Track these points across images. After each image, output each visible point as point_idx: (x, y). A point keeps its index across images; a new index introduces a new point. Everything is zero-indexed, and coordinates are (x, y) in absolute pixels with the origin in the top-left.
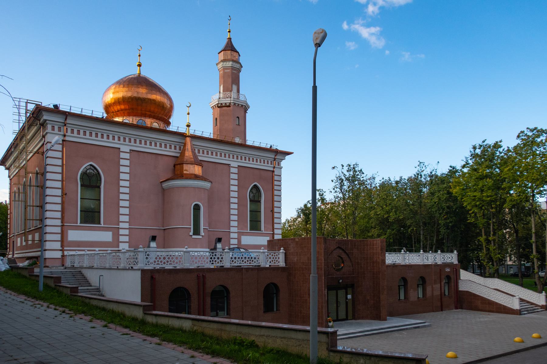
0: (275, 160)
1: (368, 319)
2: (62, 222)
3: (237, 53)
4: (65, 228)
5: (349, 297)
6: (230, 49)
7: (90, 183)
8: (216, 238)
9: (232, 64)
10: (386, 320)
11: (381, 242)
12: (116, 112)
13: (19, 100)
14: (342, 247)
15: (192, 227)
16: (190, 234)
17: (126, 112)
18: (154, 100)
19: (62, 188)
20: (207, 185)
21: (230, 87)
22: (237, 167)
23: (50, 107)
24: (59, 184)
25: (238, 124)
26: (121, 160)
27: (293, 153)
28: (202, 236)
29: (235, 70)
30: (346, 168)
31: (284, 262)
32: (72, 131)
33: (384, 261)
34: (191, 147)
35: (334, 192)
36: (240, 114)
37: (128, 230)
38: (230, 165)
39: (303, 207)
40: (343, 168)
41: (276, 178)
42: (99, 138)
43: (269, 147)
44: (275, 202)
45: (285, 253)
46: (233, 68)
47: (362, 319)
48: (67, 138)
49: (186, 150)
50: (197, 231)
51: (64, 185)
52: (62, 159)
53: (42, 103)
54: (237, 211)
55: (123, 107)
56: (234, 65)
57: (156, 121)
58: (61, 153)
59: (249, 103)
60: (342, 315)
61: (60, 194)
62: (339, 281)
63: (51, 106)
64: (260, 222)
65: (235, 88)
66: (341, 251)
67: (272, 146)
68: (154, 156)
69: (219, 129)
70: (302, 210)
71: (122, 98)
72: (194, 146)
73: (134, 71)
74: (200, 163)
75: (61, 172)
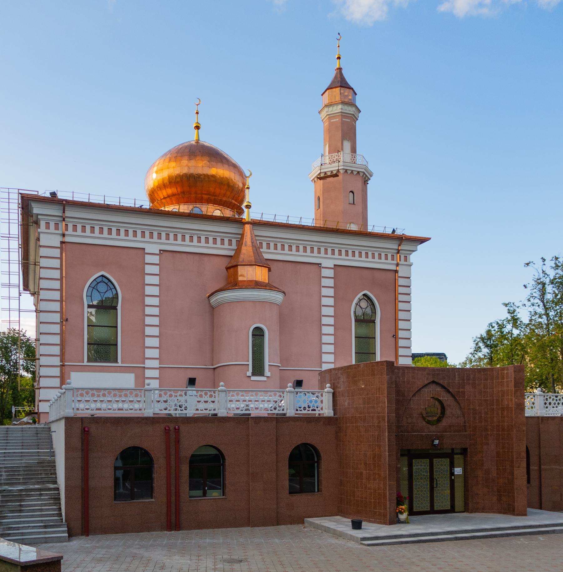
0: (398, 253)
1: (494, 512)
2: (61, 361)
3: (351, 90)
4: (67, 368)
5: (458, 471)
6: (339, 85)
7: (102, 304)
8: (295, 381)
9: (342, 109)
10: (525, 515)
11: (514, 371)
12: (161, 199)
13: (7, 190)
14: (441, 382)
15: (250, 363)
16: (248, 375)
17: (173, 198)
18: (213, 176)
19: (61, 312)
20: (277, 297)
21: (340, 144)
22: (333, 266)
23: (46, 196)
24: (56, 306)
25: (353, 203)
26: (146, 266)
27: (430, 239)
28: (267, 377)
29: (346, 117)
30: (550, 263)
31: (331, 408)
32: (75, 228)
33: (521, 407)
34: (252, 239)
35: (530, 304)
36: (357, 185)
37: (158, 371)
38: (321, 264)
39: (485, 335)
40: (545, 263)
41: (401, 282)
42: (88, 232)
43: (389, 231)
44: (400, 322)
45: (334, 394)
46: (343, 115)
47: (483, 512)
48: (67, 239)
49: (243, 245)
50: (258, 369)
51: (64, 307)
52: (61, 269)
53: (38, 192)
54: (333, 337)
55: (169, 191)
56: (346, 110)
57: (218, 208)
58: (59, 261)
59: (371, 168)
60: (442, 501)
61: (58, 320)
62: (433, 441)
63: (48, 195)
64: (374, 355)
65: (347, 145)
66: (439, 389)
67: (395, 229)
68: (197, 257)
69: (322, 213)
70: (482, 339)
71: (168, 178)
72: (257, 238)
73: (190, 137)
74: (267, 264)
75: (59, 288)
